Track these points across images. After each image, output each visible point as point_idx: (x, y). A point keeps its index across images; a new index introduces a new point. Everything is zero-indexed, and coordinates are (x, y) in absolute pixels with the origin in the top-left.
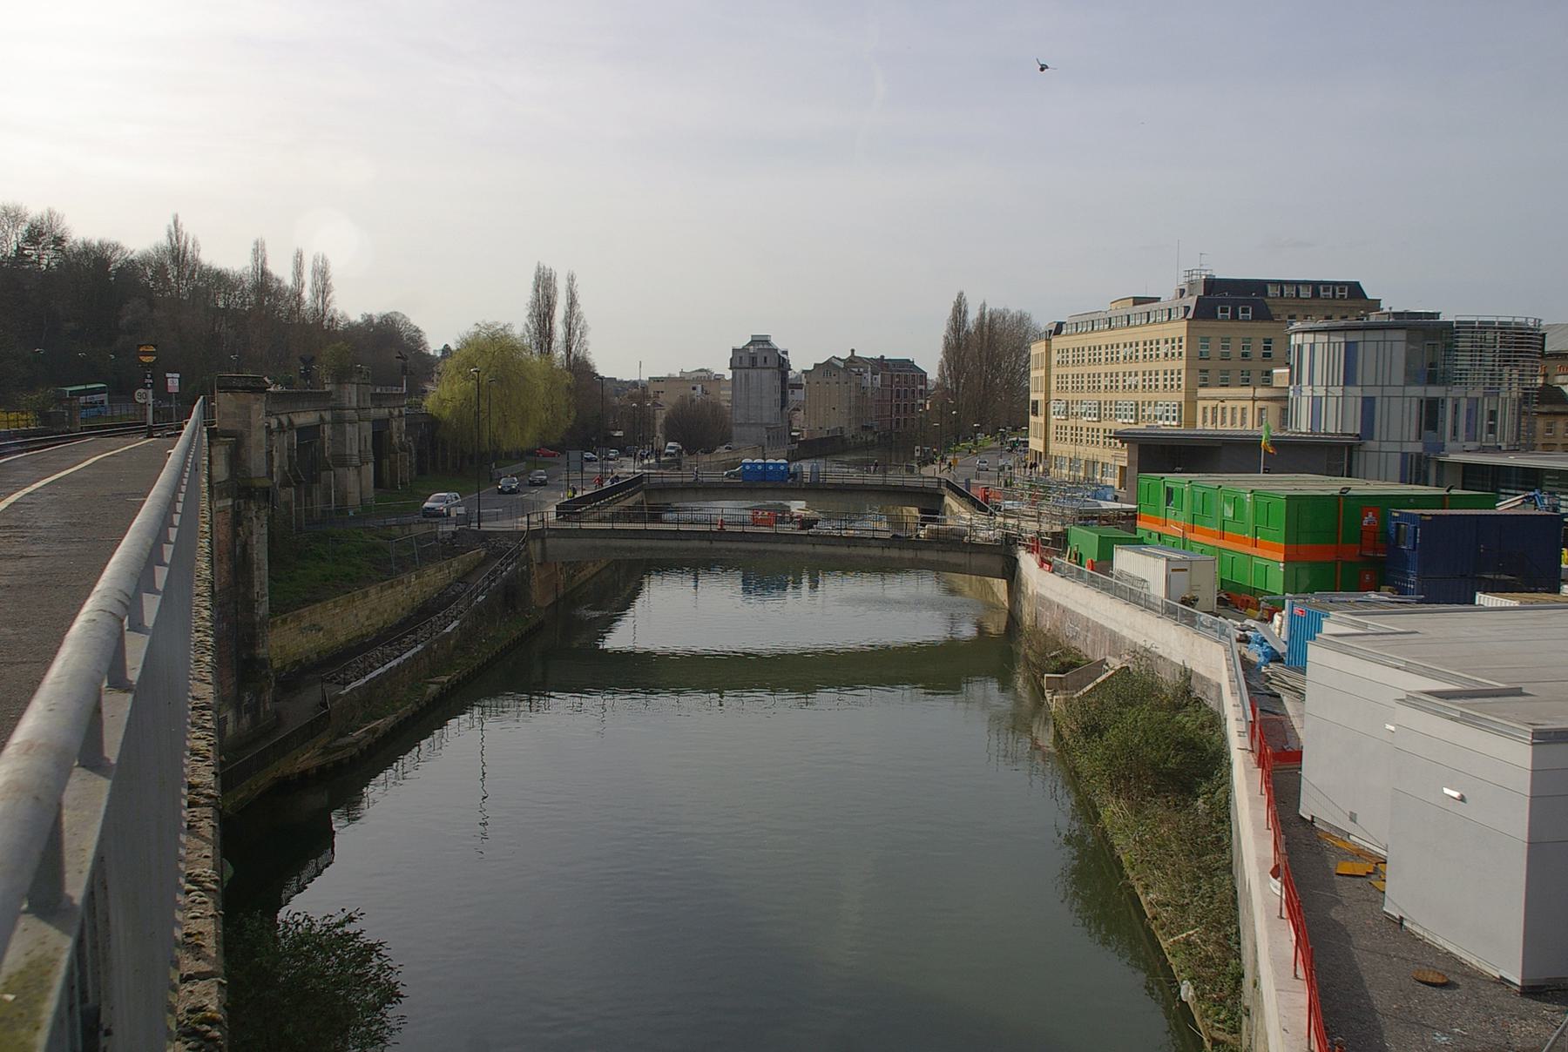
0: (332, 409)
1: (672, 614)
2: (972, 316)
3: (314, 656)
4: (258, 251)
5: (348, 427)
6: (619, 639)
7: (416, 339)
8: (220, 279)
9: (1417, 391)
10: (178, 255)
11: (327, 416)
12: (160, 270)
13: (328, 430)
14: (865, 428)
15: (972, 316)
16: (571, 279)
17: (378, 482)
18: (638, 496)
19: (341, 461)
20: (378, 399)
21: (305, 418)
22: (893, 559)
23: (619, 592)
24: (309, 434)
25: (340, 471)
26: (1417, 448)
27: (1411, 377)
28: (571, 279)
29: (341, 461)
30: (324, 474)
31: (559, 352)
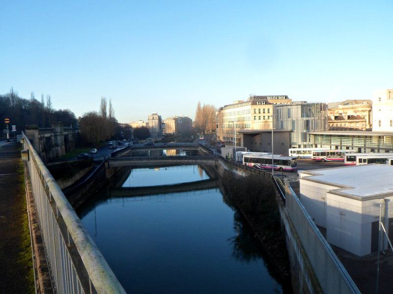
0: (54, 132)
1: (138, 177)
2: (202, 106)
3: (171, 128)
4: (32, 95)
5: (58, 137)
6: (126, 184)
7: (235, 214)
8: (24, 101)
9: (305, 119)
10: (13, 96)
11: (53, 134)
12: (8, 99)
13: (53, 138)
14: (179, 132)
15: (202, 106)
16: (110, 101)
17: (66, 150)
18: (130, 150)
19: (57, 145)
20: (65, 130)
21: (47, 135)
22: (190, 162)
23: (124, 173)
24: (49, 139)
25: (57, 148)
26: (305, 131)
27: (302, 116)
28: (110, 101)
29: (57, 145)
30: (52, 149)
31: (108, 114)
